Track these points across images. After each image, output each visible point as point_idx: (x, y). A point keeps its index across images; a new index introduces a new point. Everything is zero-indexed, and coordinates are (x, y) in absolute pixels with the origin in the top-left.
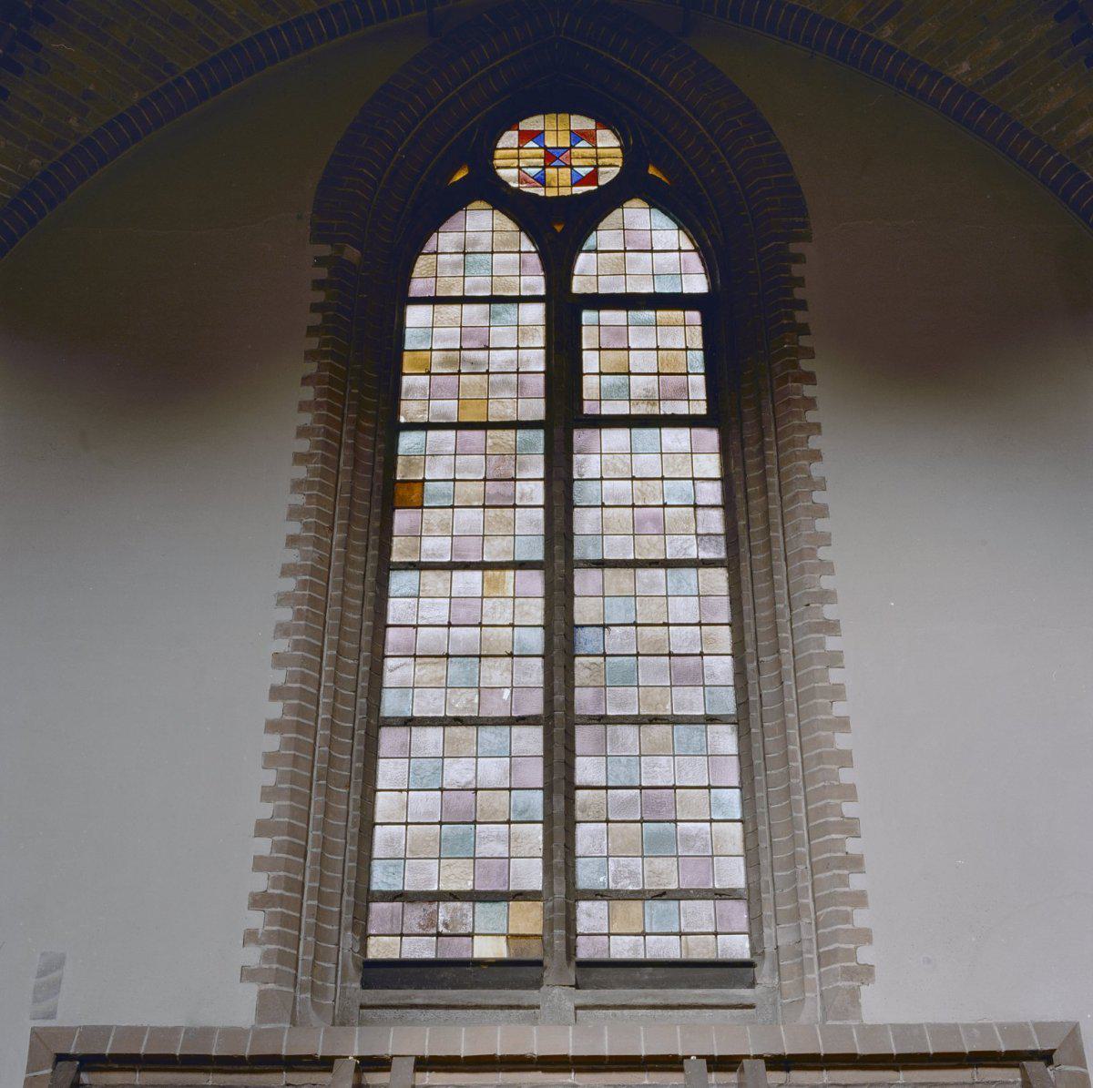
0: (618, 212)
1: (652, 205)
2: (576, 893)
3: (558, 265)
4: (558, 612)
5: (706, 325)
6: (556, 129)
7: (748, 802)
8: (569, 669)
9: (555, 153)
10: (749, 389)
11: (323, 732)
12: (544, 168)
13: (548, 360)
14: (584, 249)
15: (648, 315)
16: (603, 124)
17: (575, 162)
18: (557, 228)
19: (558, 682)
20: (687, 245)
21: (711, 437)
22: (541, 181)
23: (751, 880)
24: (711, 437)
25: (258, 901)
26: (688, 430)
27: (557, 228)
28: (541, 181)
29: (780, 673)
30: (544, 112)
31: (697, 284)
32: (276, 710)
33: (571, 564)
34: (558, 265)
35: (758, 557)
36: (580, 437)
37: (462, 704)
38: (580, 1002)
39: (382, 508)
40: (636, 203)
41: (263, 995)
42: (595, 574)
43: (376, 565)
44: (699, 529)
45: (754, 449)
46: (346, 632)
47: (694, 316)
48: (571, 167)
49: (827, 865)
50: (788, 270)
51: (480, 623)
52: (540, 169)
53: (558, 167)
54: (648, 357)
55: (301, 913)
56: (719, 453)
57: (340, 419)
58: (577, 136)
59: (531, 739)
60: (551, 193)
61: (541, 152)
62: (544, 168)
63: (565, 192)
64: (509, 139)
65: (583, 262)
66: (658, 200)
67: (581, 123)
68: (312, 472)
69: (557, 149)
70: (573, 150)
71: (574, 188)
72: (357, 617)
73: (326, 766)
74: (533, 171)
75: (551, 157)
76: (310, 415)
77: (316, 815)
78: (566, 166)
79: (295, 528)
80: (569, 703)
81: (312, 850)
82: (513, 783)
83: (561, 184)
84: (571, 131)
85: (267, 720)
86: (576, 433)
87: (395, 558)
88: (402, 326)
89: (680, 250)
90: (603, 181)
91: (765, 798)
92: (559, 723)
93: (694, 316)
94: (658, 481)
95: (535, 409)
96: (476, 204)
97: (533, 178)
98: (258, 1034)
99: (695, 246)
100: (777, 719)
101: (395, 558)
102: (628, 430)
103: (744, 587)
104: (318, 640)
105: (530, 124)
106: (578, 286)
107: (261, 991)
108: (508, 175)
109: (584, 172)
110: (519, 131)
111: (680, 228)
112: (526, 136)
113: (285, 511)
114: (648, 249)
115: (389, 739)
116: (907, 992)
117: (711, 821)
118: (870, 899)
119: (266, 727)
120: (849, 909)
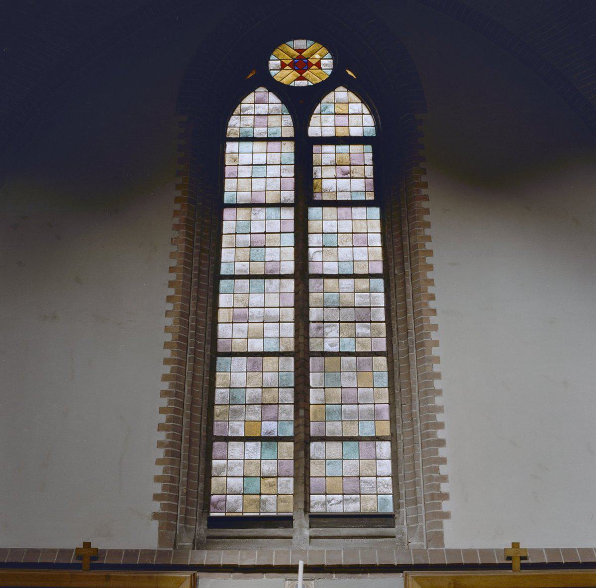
0: (332, 94)
2: (309, 439)
3: (301, 121)
4: (302, 413)
7: (392, 394)
8: (307, 468)
10: (393, 193)
11: (186, 420)
13: (296, 171)
14: (314, 113)
18: (301, 103)
19: (302, 332)
20: (366, 111)
21: (375, 212)
23: (392, 416)
24: (375, 212)
25: (164, 394)
26: (365, 208)
27: (301, 103)
29: (405, 280)
32: (168, 353)
34: (301, 121)
35: (401, 326)
36: (314, 212)
38: (313, 534)
39: (210, 369)
40: (341, 88)
41: (171, 384)
42: (321, 444)
43: (204, 467)
44: (370, 254)
45: (397, 240)
47: (369, 148)
49: (429, 444)
50: (432, 384)
51: (265, 245)
54: (346, 173)
55: (178, 503)
56: (375, 126)
57: (191, 254)
59: (287, 448)
65: (314, 120)
68: (173, 353)
72: (203, 351)
73: (197, 287)
77: (184, 471)
79: (172, 292)
80: (307, 345)
81: (185, 428)
82: (279, 236)
86: (309, 208)
87: (223, 272)
88: (224, 153)
89: (363, 114)
91: (397, 354)
92: (303, 440)
93: (369, 148)
94: (351, 239)
95: (289, 196)
98: (161, 554)
99: (370, 111)
100: (402, 302)
101: (223, 272)
103: (395, 381)
104: (181, 399)
106: (313, 131)
107: (166, 450)
114: (345, 114)
115: (224, 284)
116: (469, 530)
117: (374, 404)
118: (450, 497)
120: (437, 465)
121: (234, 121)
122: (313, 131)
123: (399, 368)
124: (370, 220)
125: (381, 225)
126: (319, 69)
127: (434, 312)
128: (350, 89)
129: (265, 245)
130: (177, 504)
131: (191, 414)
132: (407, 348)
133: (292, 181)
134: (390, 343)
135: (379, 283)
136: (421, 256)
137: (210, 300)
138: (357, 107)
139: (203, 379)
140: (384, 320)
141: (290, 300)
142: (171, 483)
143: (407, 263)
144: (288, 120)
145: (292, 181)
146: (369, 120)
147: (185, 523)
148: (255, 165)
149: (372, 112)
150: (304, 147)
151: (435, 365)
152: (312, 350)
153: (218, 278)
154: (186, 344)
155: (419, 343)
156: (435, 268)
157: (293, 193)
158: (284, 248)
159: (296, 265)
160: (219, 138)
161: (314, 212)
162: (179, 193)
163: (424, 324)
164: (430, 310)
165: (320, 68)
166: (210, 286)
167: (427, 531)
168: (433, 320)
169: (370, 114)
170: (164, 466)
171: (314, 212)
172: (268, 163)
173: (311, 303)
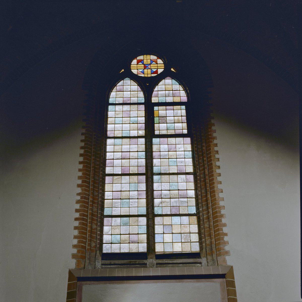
1: (131, 79)
5: (186, 110)
6: (147, 59)
9: (147, 65)
10: (199, 132)
11: (88, 234)
12: (144, 69)
15: (172, 107)
16: (159, 57)
17: (152, 68)
18: (148, 85)
21: (188, 140)
22: (143, 73)
24: (188, 140)
27: (148, 85)
28: (143, 73)
30: (143, 55)
31: (184, 99)
33: (153, 174)
37: (125, 211)
46: (95, 202)
47: (184, 107)
48: (151, 69)
51: (129, 198)
52: (143, 70)
53: (147, 69)
54: (174, 119)
58: (152, 61)
60: (146, 76)
61: (143, 66)
62: (144, 69)
63: (149, 76)
64: (135, 62)
66: (173, 76)
67: (153, 57)
69: (147, 64)
70: (151, 65)
71: (152, 75)
72: (97, 201)
74: (141, 70)
75: (145, 67)
76: (84, 136)
78: (149, 69)
83: (148, 73)
84: (151, 60)
85: (79, 157)
90: (159, 73)
93: (184, 107)
94: (177, 154)
96: (168, 78)
97: (141, 72)
102: (155, 131)
105: (139, 58)
106: (154, 100)
108: (135, 71)
109: (154, 70)
110: (137, 60)
111: (180, 84)
112: (139, 62)
113: (78, 163)
114: (169, 89)
119: (77, 195)
121: (113, 94)
122: (154, 100)
123: (202, 205)
124: (184, 146)
125: (191, 140)
126: (156, 64)
127: (219, 167)
128: (173, 78)
129: (129, 198)
130: (86, 236)
131: (91, 234)
132: (206, 203)
133: (144, 131)
134: (197, 208)
135: (191, 177)
136: (215, 185)
137: (99, 228)
138: (177, 86)
139: (96, 242)
140: (194, 197)
141: (143, 147)
142: (81, 237)
143: (207, 177)
144: (141, 94)
145: (144, 131)
146: (183, 93)
147: (91, 233)
148: (123, 116)
149: (185, 90)
150: (149, 107)
151: (227, 258)
152: (156, 213)
153: (103, 216)
154: (86, 241)
155: (215, 225)
156: (228, 234)
157: (144, 131)
158: (140, 192)
159: (145, 99)
160: (104, 104)
161: (155, 140)
162: (84, 131)
163: (215, 189)
164: (216, 158)
165: (157, 64)
166: (99, 216)
167: (207, 153)
168: (219, 179)
169: (184, 90)
170: (81, 204)
171: (155, 140)
172: (130, 233)
173: (155, 196)
